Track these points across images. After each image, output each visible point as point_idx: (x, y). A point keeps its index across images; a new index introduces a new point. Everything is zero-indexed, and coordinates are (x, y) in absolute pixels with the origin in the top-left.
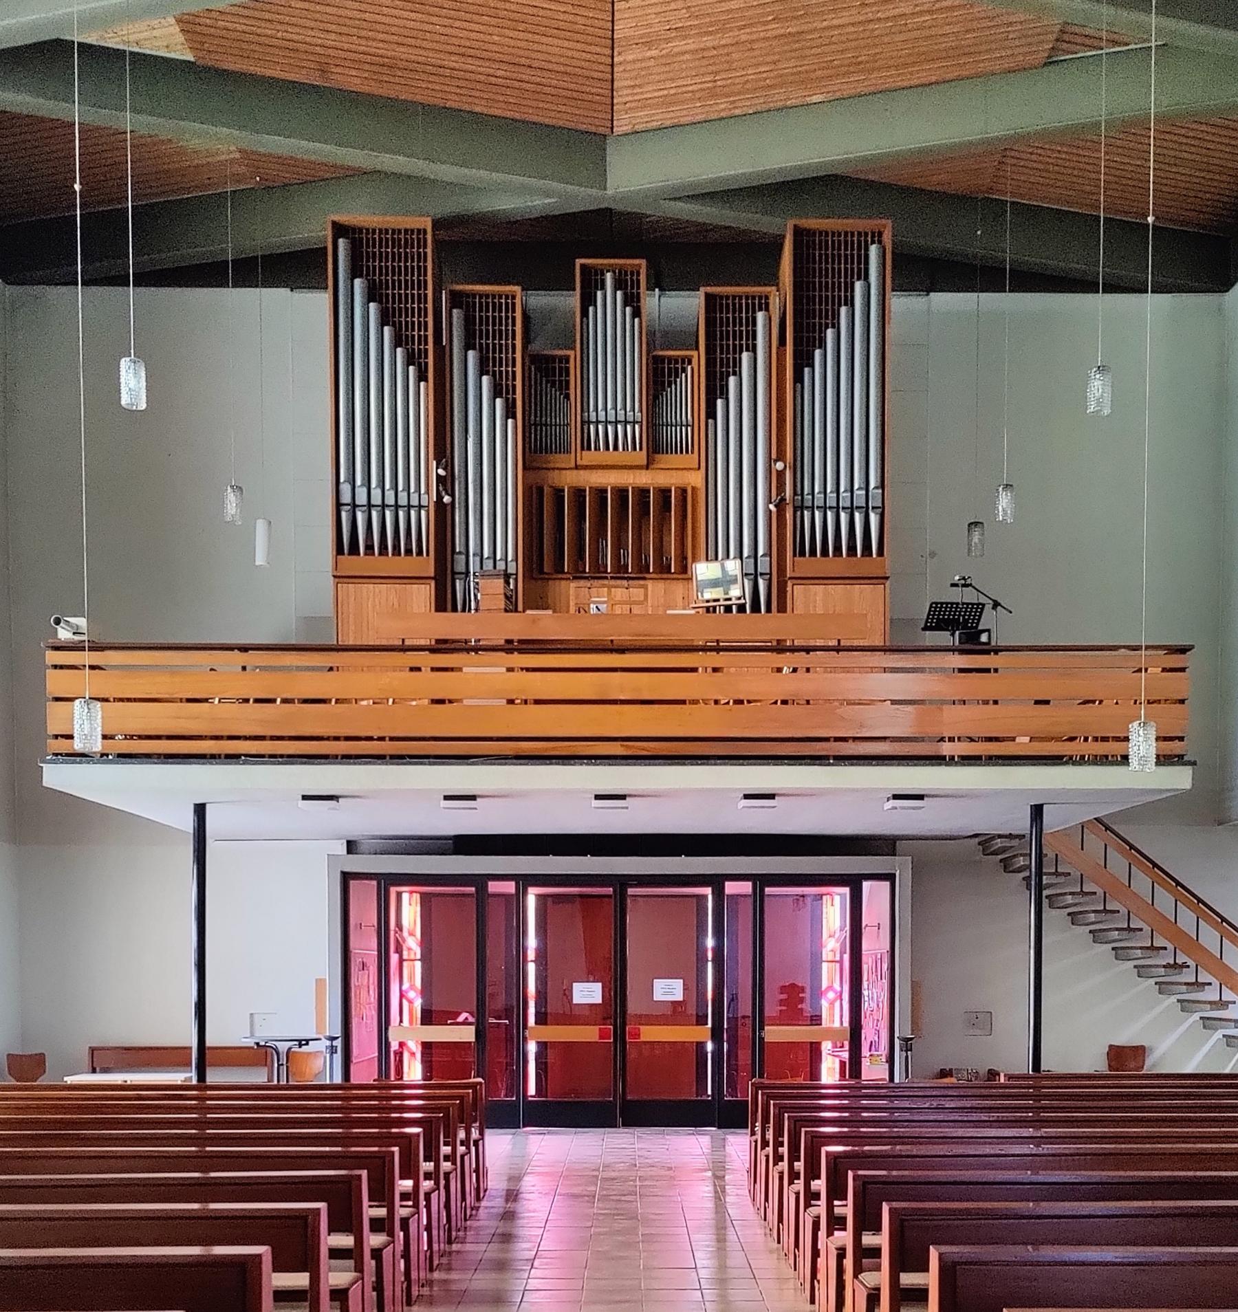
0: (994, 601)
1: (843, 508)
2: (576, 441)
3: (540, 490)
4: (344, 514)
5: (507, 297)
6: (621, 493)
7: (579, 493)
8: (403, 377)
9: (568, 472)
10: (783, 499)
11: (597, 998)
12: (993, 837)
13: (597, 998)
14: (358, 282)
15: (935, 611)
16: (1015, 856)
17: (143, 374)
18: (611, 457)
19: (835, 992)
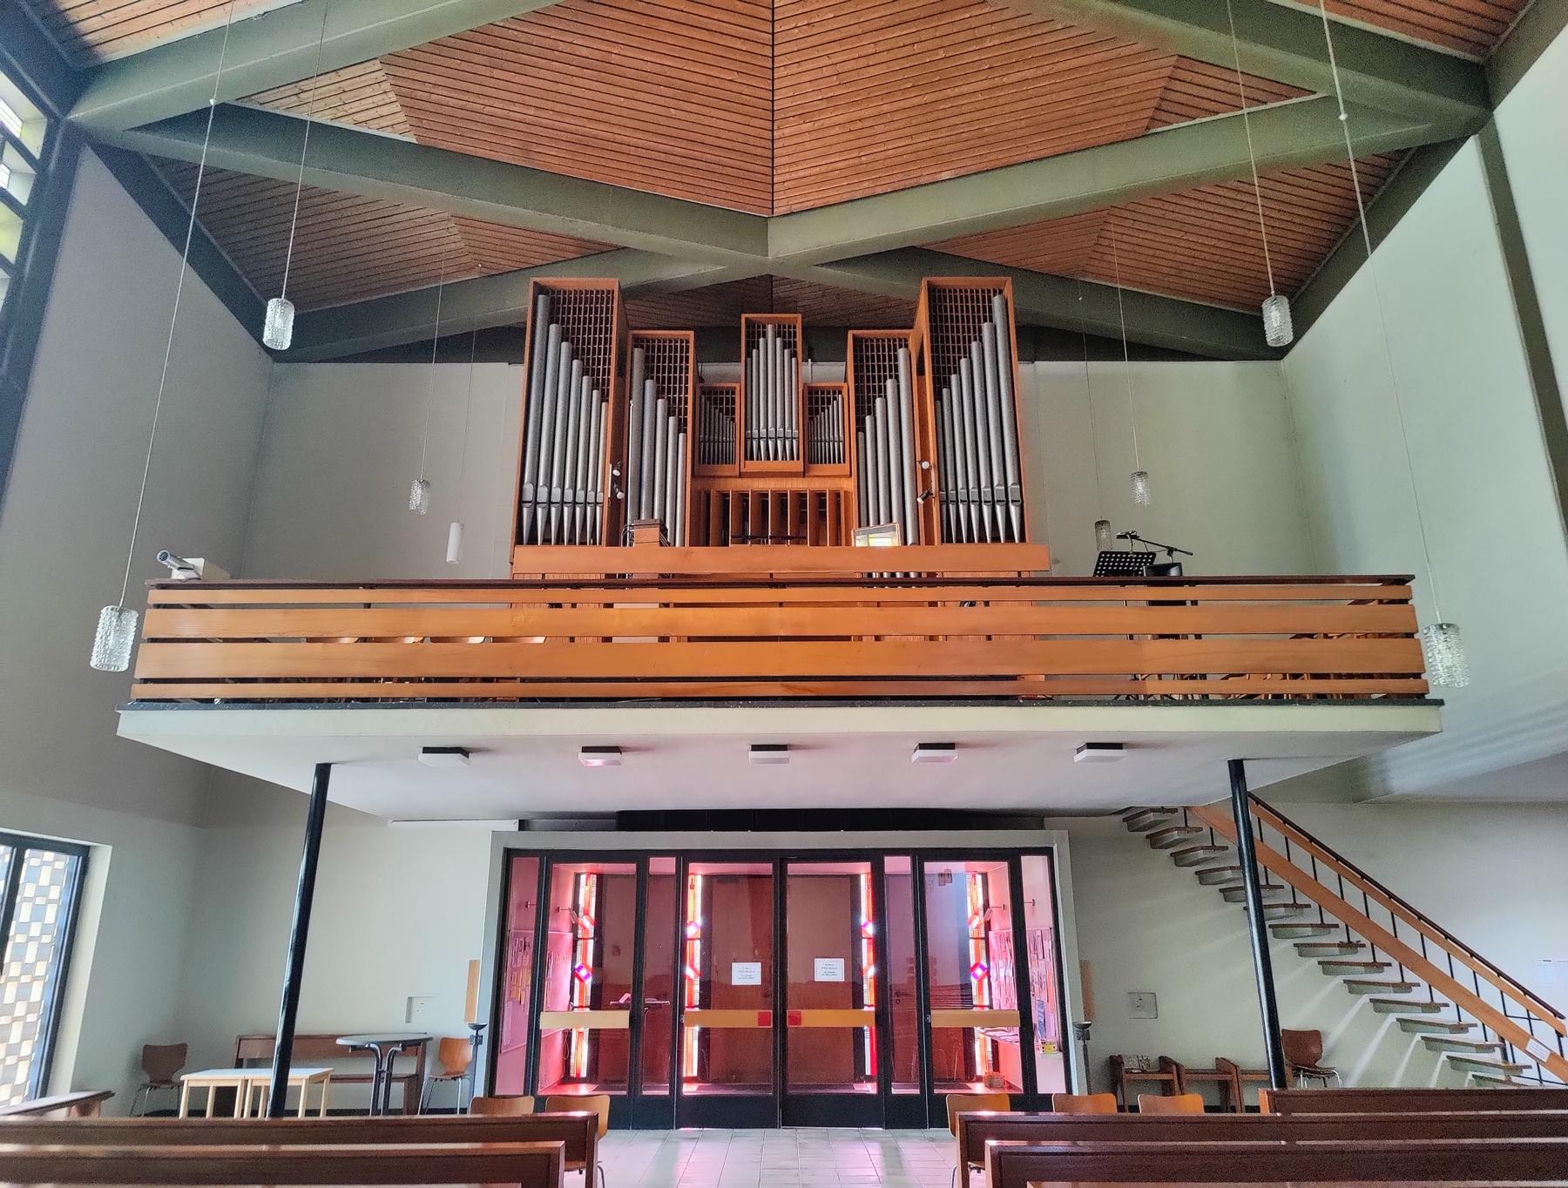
0: (1167, 547)
2: (740, 451)
3: (708, 495)
4: (525, 510)
5: (682, 342)
6: (781, 497)
8: (587, 400)
9: (733, 479)
10: (930, 494)
11: (756, 979)
12: (1145, 812)
13: (756, 979)
14: (553, 327)
15: (1103, 562)
16: (1168, 831)
17: (292, 317)
18: (772, 466)
19: (982, 967)
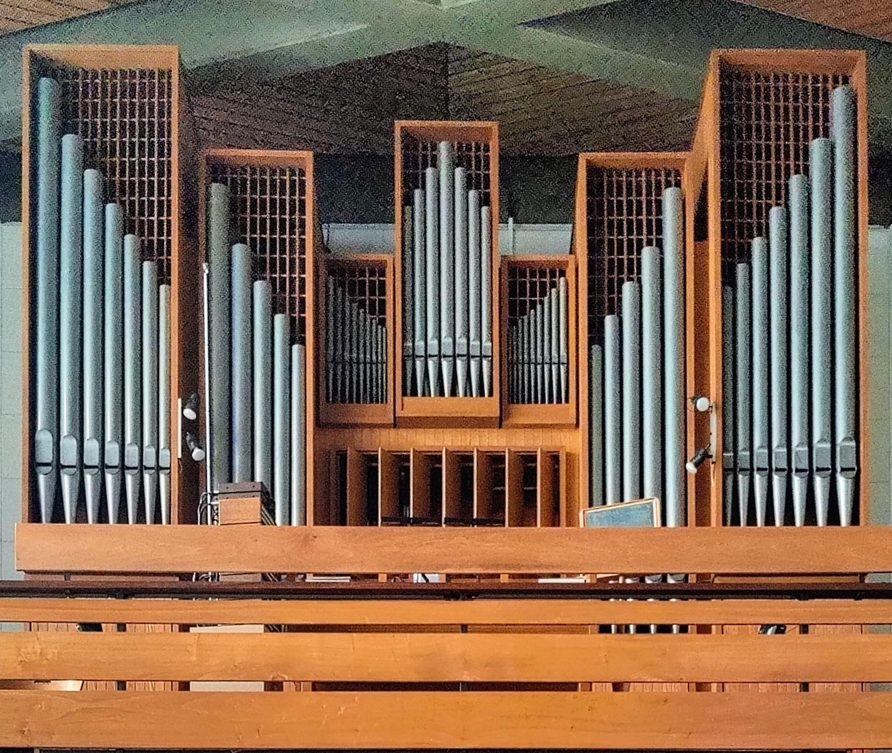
1: (797, 470)
4: (42, 479)
6: (462, 460)
7: (400, 461)
10: (707, 456)
18: (447, 406)
